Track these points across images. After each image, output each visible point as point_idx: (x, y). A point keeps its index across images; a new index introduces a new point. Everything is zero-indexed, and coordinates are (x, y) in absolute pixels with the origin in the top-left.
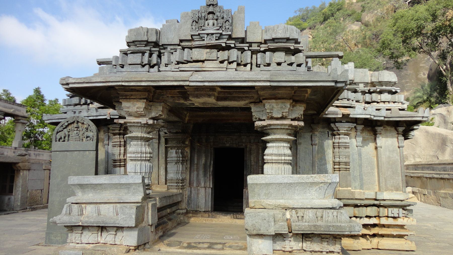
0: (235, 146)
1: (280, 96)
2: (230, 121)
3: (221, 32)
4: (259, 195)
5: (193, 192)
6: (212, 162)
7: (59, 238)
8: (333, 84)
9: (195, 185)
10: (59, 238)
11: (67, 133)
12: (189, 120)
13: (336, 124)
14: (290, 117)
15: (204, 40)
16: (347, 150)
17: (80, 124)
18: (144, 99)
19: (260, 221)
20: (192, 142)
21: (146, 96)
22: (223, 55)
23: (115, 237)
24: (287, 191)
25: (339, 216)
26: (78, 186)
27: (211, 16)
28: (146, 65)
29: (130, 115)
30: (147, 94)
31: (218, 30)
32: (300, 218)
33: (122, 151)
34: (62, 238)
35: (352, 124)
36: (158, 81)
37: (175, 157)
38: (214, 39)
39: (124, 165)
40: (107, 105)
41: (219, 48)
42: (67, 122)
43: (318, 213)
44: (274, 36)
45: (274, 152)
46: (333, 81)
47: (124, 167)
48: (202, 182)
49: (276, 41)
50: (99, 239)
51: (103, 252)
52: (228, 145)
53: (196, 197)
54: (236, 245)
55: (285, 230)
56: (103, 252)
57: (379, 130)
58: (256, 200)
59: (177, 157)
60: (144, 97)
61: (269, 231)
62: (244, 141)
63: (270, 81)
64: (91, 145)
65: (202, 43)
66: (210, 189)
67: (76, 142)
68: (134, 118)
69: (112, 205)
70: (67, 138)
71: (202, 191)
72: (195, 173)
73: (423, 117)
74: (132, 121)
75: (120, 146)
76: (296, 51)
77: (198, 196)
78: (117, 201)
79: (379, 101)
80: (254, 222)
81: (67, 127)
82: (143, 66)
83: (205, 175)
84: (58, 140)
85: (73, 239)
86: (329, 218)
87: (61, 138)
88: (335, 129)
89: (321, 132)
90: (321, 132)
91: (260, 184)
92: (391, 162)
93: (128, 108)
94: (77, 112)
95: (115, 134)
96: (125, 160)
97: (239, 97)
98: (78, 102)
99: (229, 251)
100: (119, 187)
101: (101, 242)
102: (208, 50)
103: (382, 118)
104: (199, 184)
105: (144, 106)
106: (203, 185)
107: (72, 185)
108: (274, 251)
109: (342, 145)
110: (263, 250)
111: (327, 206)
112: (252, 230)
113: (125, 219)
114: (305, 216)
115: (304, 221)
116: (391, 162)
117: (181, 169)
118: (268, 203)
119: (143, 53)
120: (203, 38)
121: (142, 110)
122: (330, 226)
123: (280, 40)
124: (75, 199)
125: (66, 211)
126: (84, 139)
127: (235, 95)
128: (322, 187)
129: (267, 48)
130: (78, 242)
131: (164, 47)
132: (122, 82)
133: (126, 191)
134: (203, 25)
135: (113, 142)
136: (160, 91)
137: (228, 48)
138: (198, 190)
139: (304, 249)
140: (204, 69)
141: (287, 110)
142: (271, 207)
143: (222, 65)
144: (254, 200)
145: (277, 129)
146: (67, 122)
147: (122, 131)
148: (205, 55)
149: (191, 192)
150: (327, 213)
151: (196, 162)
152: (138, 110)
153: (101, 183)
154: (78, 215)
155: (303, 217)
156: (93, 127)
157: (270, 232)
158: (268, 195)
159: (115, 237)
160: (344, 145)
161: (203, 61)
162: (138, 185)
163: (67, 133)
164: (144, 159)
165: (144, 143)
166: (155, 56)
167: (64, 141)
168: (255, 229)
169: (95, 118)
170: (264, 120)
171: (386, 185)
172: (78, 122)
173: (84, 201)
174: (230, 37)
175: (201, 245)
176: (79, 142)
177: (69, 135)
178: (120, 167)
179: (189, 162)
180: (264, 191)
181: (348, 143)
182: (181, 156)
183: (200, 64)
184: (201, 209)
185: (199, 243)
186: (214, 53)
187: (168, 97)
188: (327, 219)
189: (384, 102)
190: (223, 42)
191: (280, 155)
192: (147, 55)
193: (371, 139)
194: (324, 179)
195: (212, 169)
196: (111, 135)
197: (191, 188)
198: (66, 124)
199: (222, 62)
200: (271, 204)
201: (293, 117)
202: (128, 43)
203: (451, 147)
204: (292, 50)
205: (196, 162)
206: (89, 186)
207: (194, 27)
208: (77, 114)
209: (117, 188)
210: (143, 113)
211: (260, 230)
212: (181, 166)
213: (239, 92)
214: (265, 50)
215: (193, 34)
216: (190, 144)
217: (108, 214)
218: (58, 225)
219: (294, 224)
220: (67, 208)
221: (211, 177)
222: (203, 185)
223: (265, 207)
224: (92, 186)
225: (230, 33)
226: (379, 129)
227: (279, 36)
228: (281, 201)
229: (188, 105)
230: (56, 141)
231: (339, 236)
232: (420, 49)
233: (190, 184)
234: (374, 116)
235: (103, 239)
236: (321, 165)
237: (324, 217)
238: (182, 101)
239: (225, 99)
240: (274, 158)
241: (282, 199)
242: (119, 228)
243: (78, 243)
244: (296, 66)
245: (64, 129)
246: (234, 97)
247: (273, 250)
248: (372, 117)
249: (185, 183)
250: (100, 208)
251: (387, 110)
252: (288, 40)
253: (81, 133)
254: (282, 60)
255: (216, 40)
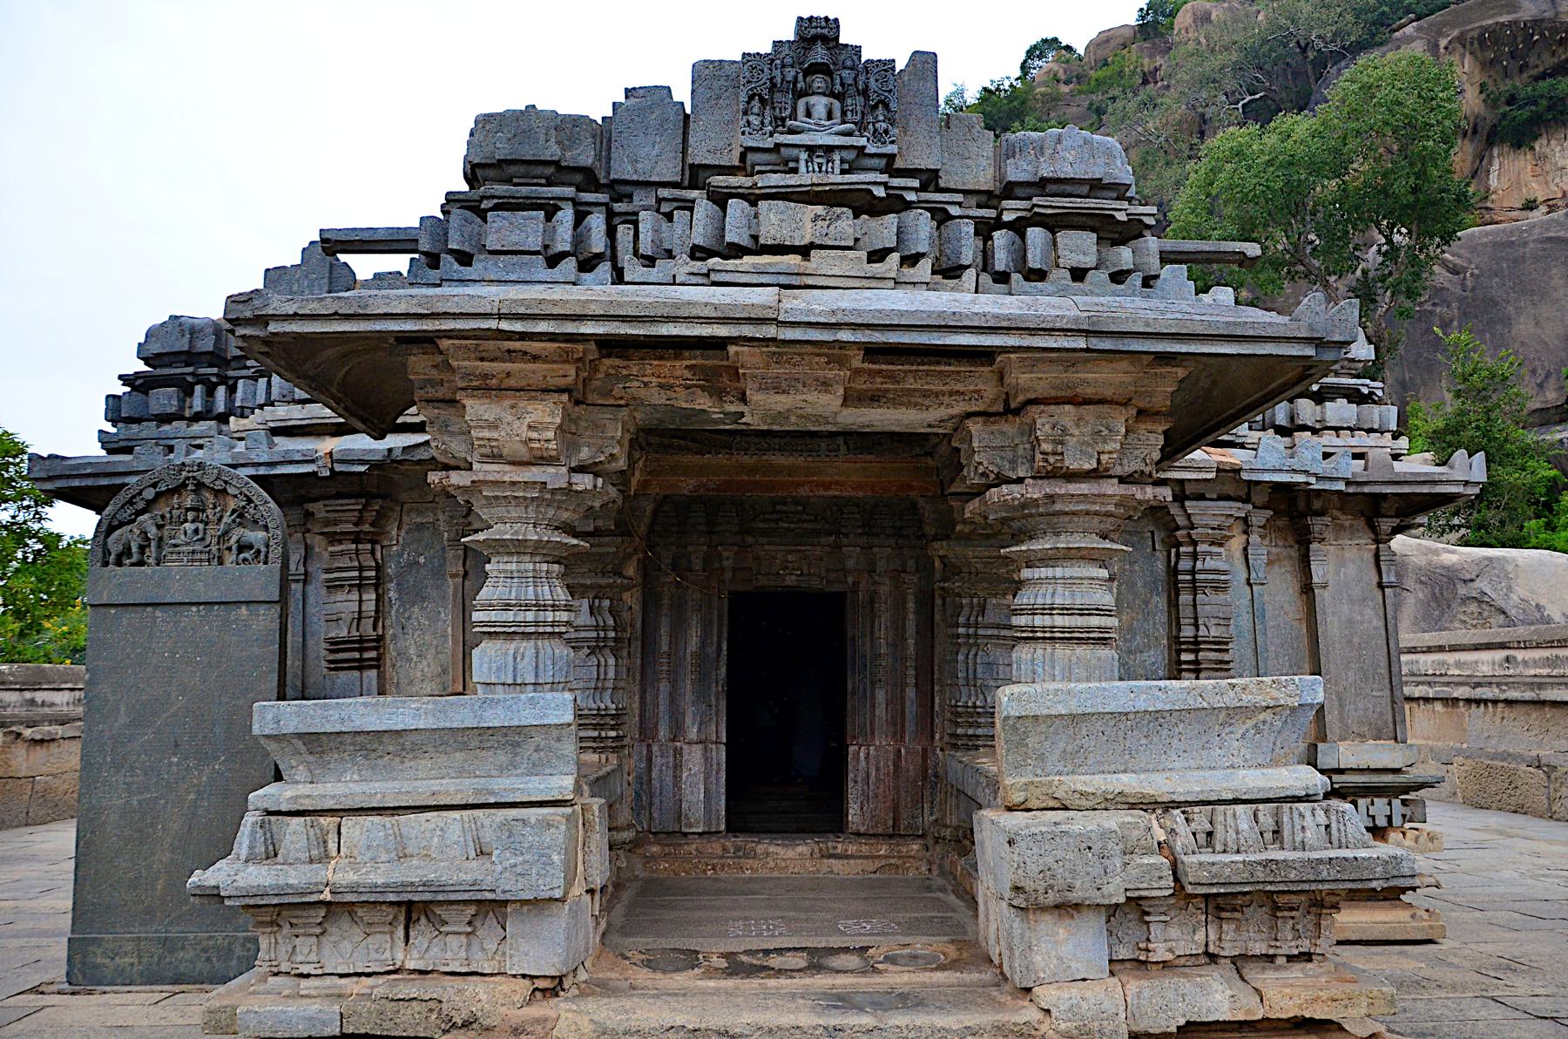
0: (816, 584)
1: (1089, 391)
2: (804, 491)
3: (862, 142)
4: (1041, 758)
5: (657, 761)
6: (725, 647)
7: (127, 960)
8: (1310, 351)
9: (663, 733)
10: (127, 960)
11: (153, 532)
12: (644, 484)
13: (1187, 503)
14: (1118, 471)
15: (795, 171)
16: (1222, 596)
17: (209, 498)
18: (560, 391)
19: (1070, 856)
20: (648, 570)
21: (570, 380)
22: (884, 229)
23: (469, 945)
24: (1144, 741)
25: (1334, 826)
26: (299, 744)
27: (819, 82)
28: (563, 255)
29: (495, 457)
30: (572, 372)
31: (849, 134)
32: (1202, 838)
33: (370, 607)
34: (139, 957)
35: (1240, 505)
36: (652, 320)
37: (586, 628)
38: (837, 171)
39: (378, 659)
40: (360, 418)
41: (865, 205)
42: (154, 485)
43: (1260, 815)
44: (1046, 171)
45: (1058, 601)
46: (1308, 340)
47: (377, 667)
48: (688, 721)
49: (1051, 188)
50: (400, 956)
51: (432, 1004)
52: (790, 581)
53: (669, 780)
54: (907, 951)
55: (1163, 883)
56: (432, 1004)
57: (1317, 528)
58: (1032, 778)
59: (597, 628)
60: (562, 382)
61: (1105, 890)
62: (851, 564)
63: (1087, 333)
64: (260, 579)
65: (791, 180)
66: (723, 748)
67: (193, 569)
68: (507, 468)
69: (456, 814)
70: (152, 550)
71: (694, 758)
72: (664, 686)
73: (1467, 483)
74: (506, 478)
75: (360, 587)
76: (1130, 232)
77: (677, 778)
78: (471, 801)
79: (1318, 426)
80: (1050, 860)
81: (149, 505)
82: (553, 261)
83: (701, 696)
84: (112, 558)
85: (283, 955)
86: (1308, 834)
87: (127, 552)
88: (1181, 521)
89: (1130, 533)
90: (1130, 533)
91: (1049, 716)
92: (1356, 640)
93: (493, 426)
94: (181, 446)
95: (333, 538)
96: (380, 639)
97: (926, 394)
98: (172, 408)
99: (906, 978)
100: (474, 743)
101: (411, 965)
102: (820, 209)
103: (1341, 486)
104: (677, 731)
105: (558, 420)
106: (693, 733)
107: (267, 737)
108: (1117, 967)
109: (1206, 581)
110: (1073, 965)
111: (1289, 793)
112: (1042, 890)
113: (519, 869)
114: (1219, 828)
115: (1219, 847)
116: (1356, 640)
117: (611, 674)
118: (1080, 787)
119: (551, 211)
120: (791, 165)
121: (551, 435)
122: (1320, 861)
123: (1069, 189)
124: (289, 794)
125: (251, 847)
126: (230, 558)
127: (910, 383)
128: (1264, 722)
129: (1029, 214)
130: (304, 969)
131: (620, 189)
132: (500, 316)
133: (503, 757)
134: (788, 112)
135: (328, 571)
136: (617, 362)
137: (896, 204)
138: (678, 752)
139: (1211, 949)
140: (810, 281)
141: (1118, 446)
142: (1089, 804)
143: (877, 268)
144: (1024, 780)
145: (1074, 513)
146: (154, 485)
147: (367, 528)
148: (809, 225)
149: (650, 760)
150: (1296, 815)
151: (665, 648)
152: (534, 435)
153: (400, 727)
154: (311, 861)
155: (1210, 834)
156: (269, 508)
157: (1111, 895)
158: (1075, 760)
159: (469, 945)
160: (1213, 581)
161: (805, 251)
162: (555, 733)
163: (153, 532)
164: (549, 629)
165: (545, 567)
166: (597, 222)
167: (141, 563)
168: (1052, 887)
169: (262, 471)
170: (1020, 481)
171: (1342, 719)
172: (200, 486)
173: (330, 804)
174: (889, 165)
175: (775, 961)
176: (205, 566)
177: (161, 539)
178: (360, 669)
179: (637, 646)
180: (1062, 745)
181: (1225, 573)
182: (611, 622)
183: (793, 260)
184: (691, 826)
185: (767, 952)
186: (846, 225)
187: (646, 384)
188: (1298, 839)
189: (1337, 429)
190: (873, 181)
191: (1083, 612)
192: (566, 215)
193: (1291, 557)
194: (1275, 693)
195: (723, 670)
196: (317, 542)
197: (649, 746)
198: (149, 494)
199: (877, 256)
200: (1090, 790)
201: (1129, 467)
202: (474, 166)
203: (1421, 595)
204: (1119, 222)
205: (665, 648)
206: (348, 739)
207: (755, 120)
208: (177, 458)
209: (464, 747)
210: (552, 445)
211: (1070, 888)
212: (612, 661)
213: (927, 373)
214: (1018, 218)
215: (751, 144)
216: (640, 580)
217: (440, 854)
218: (227, 902)
219: (1194, 859)
220: (253, 832)
221: (723, 703)
222: (693, 733)
223: (1067, 803)
224: (359, 739)
225: (891, 149)
226: (1317, 524)
227: (1067, 171)
228: (1124, 777)
229: (715, 422)
230: (106, 564)
231: (1334, 899)
232: (1295, 264)
233: (647, 732)
234: (1319, 478)
235: (415, 954)
236: (1130, 652)
237: (1286, 833)
238: (703, 402)
239: (874, 399)
240: (1059, 621)
241: (1125, 771)
242: (490, 908)
243: (308, 976)
244: (1139, 283)
245: (140, 513)
246: (910, 392)
247: (1111, 961)
248: (1313, 480)
249: (626, 728)
250: (404, 830)
251: (1356, 456)
252: (1096, 186)
253: (214, 531)
254: (1089, 260)
255: (843, 172)
